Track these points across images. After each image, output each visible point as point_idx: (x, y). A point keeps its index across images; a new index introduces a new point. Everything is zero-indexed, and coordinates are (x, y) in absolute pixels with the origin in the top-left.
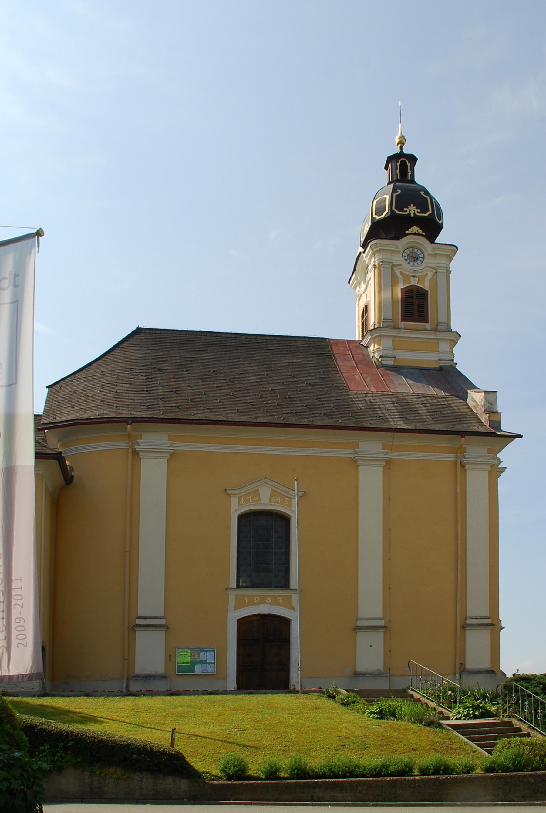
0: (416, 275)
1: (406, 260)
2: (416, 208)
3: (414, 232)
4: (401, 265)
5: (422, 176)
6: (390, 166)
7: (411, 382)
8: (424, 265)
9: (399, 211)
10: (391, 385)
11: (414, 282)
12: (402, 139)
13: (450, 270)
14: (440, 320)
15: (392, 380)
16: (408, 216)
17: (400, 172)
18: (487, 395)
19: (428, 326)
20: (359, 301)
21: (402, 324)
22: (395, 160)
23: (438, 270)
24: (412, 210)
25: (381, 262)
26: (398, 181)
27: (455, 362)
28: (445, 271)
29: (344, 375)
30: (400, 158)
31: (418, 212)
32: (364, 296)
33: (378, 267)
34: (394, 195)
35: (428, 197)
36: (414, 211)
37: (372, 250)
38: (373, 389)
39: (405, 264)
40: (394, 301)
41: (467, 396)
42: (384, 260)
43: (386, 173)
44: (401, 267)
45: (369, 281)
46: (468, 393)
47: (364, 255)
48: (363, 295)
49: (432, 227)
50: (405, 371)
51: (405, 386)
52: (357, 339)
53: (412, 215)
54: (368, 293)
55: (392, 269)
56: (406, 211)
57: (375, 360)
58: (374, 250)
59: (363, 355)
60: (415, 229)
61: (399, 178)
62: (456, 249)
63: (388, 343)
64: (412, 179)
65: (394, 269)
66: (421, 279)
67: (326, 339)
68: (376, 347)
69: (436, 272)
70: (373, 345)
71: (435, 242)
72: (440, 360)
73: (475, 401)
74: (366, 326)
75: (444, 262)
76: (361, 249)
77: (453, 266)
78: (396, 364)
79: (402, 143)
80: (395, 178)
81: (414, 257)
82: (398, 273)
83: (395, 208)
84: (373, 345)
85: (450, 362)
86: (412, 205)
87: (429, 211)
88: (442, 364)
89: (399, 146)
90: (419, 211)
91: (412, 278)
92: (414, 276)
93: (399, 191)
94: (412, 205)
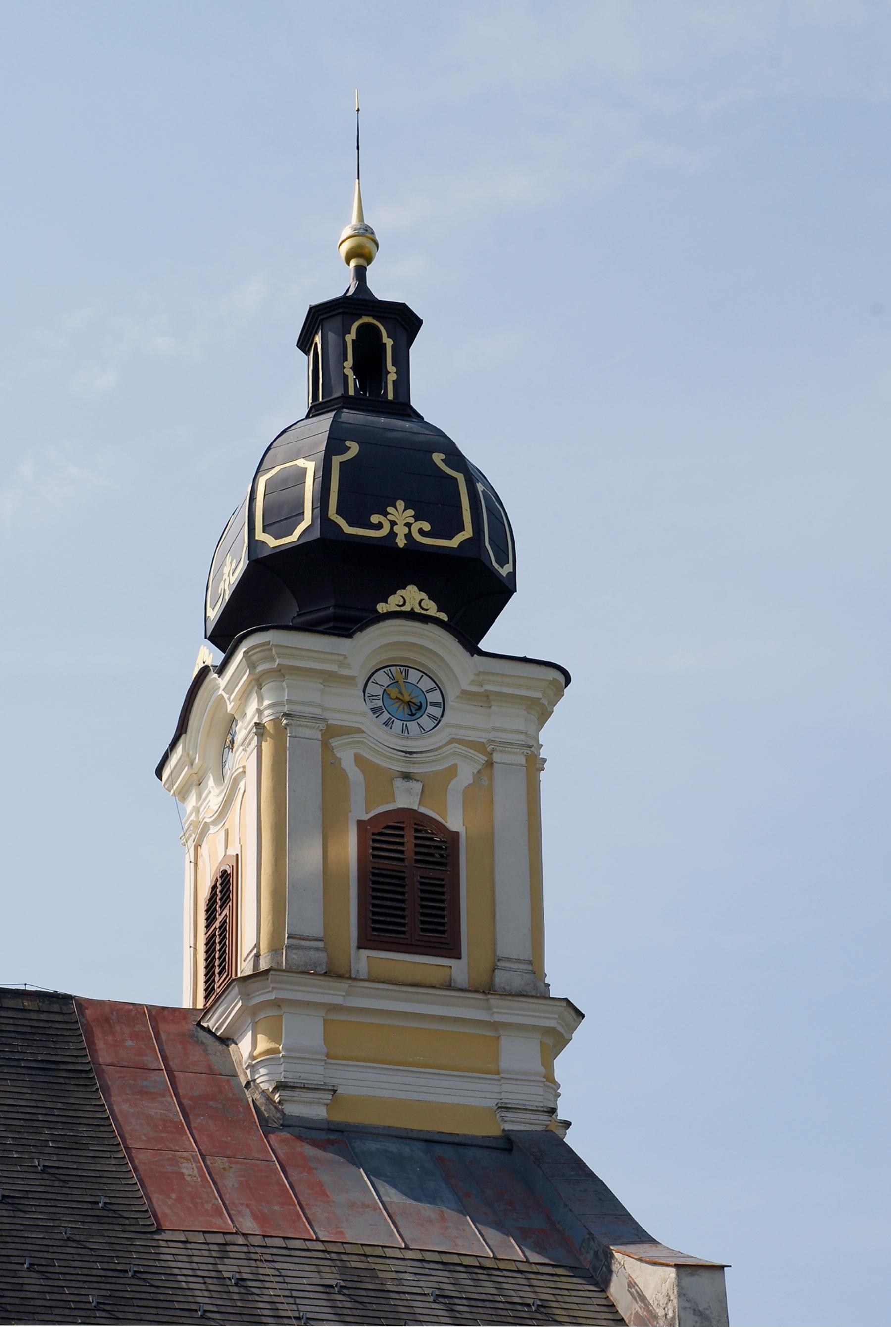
0: (413, 770)
1: (375, 710)
2: (417, 518)
3: (407, 608)
4: (360, 731)
5: (438, 385)
6: (318, 339)
7: (394, 1196)
8: (440, 736)
9: (351, 524)
10: (317, 1211)
11: (406, 798)
12: (363, 240)
13: (543, 754)
14: (503, 950)
15: (320, 1184)
16: (380, 546)
17: (355, 368)
18: (688, 1280)
19: (459, 970)
20: (197, 847)
21: (364, 960)
22: (336, 322)
23: (496, 757)
24: (400, 523)
25: (286, 715)
26: (346, 402)
27: (562, 1115)
28: (523, 761)
29: (141, 1158)
30: (359, 316)
31: (421, 532)
32: (216, 834)
33: (278, 733)
34: (336, 460)
35: (460, 477)
36: (409, 525)
37: (252, 666)
38: (248, 1225)
39: (372, 726)
40: (329, 874)
41: (610, 1272)
42: (297, 709)
43: (302, 363)
44: (357, 737)
45: (236, 781)
46: (612, 1256)
47: (223, 682)
48: (213, 829)
49: (474, 588)
50: (373, 1146)
51: (369, 1215)
52: (187, 1004)
53: (401, 542)
54: (232, 819)
55: (325, 745)
56: (379, 526)
57: (257, 1096)
58: (260, 668)
59: (212, 1072)
60: (411, 596)
61: (352, 392)
62: (562, 679)
63: (308, 1031)
64: (401, 399)
65: (334, 743)
66: (435, 785)
67: (67, 998)
68: (264, 1044)
69: (490, 764)
70: (248, 1037)
71: (483, 645)
72: (504, 1108)
73: (642, 1298)
74: (223, 953)
75: (519, 724)
76: (210, 655)
77: (552, 738)
78: (340, 1117)
79: (362, 255)
80: (337, 393)
81: (407, 704)
82: (346, 759)
83: (339, 512)
84: (248, 1037)
85: (544, 1117)
86: (401, 504)
87: (463, 529)
88: (515, 1123)
89: (353, 263)
90: (427, 526)
91: (399, 783)
92: (407, 776)
93: (354, 449)
94: (401, 504)
